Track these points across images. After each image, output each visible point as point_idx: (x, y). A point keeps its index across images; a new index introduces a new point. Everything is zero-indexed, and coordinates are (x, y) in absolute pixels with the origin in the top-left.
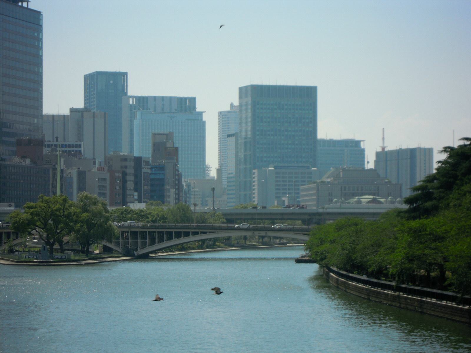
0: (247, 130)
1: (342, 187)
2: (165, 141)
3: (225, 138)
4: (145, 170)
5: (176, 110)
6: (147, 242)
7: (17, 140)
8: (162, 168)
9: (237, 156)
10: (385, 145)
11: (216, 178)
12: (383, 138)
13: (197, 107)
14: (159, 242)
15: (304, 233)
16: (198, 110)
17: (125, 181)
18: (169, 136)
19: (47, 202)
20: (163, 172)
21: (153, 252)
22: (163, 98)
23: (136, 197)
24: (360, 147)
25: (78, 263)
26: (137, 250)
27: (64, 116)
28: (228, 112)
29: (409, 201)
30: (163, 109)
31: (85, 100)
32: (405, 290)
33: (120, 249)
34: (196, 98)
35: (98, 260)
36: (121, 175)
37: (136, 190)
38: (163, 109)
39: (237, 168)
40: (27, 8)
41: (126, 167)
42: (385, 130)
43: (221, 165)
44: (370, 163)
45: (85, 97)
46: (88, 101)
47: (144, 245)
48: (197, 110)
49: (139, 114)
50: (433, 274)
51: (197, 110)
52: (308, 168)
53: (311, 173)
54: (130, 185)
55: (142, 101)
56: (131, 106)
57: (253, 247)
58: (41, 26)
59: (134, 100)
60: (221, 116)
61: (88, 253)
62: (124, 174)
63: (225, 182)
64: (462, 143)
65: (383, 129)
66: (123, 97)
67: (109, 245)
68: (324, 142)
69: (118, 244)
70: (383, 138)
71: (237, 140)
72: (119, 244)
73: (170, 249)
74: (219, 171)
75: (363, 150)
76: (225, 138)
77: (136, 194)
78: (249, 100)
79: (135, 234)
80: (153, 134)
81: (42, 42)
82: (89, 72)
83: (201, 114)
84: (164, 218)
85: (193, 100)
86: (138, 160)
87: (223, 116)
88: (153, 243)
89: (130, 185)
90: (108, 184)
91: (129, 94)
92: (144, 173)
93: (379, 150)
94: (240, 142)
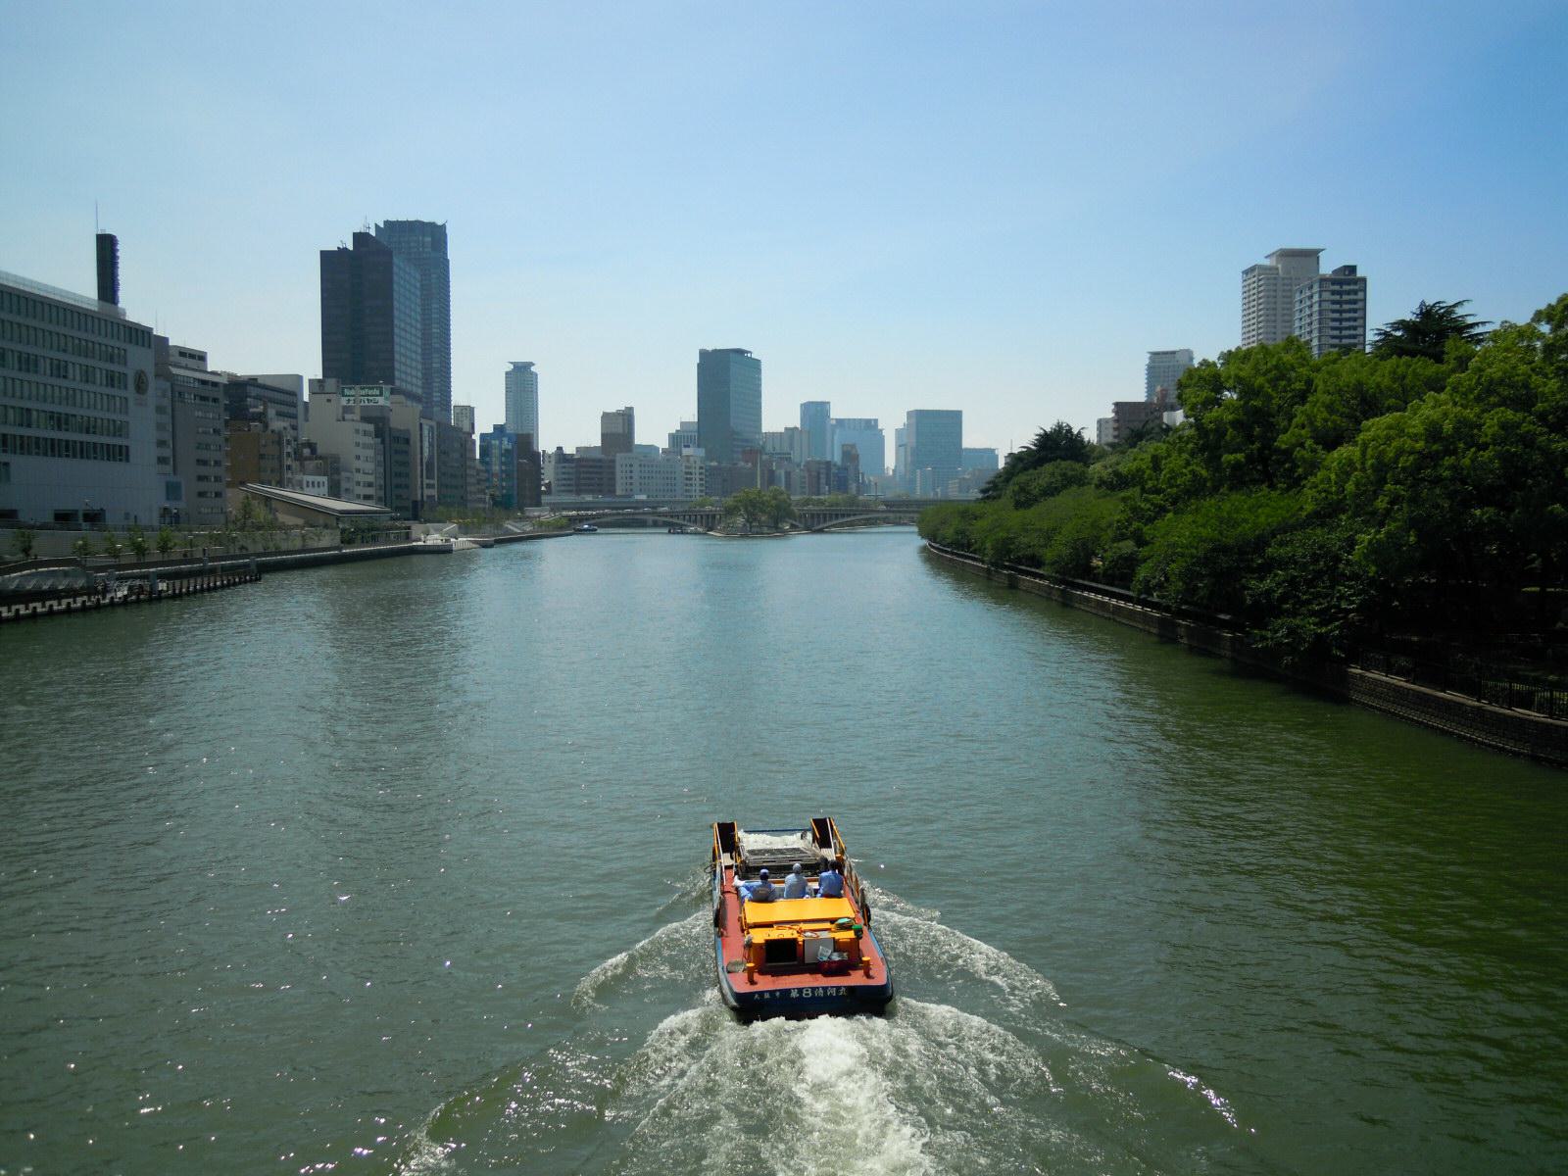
4: (834, 470)
7: (85, 521)
8: (846, 469)
16: (880, 427)
17: (819, 478)
18: (853, 446)
19: (747, 493)
21: (827, 528)
22: (849, 419)
25: (770, 536)
27: (781, 433)
29: (983, 491)
32: (956, 554)
33: (802, 526)
35: (784, 534)
37: (827, 484)
43: (896, 467)
47: (819, 523)
49: (838, 431)
52: (955, 468)
53: (957, 472)
54: (823, 481)
55: (840, 422)
56: (832, 425)
57: (905, 524)
61: (777, 528)
62: (819, 473)
63: (898, 479)
64: (1020, 450)
67: (794, 523)
68: (966, 449)
69: (800, 522)
73: (834, 526)
74: (894, 471)
78: (914, 420)
79: (812, 516)
83: (881, 430)
84: (837, 505)
85: (876, 421)
86: (828, 463)
88: (825, 521)
89: (823, 481)
91: (831, 417)
94: (909, 450)
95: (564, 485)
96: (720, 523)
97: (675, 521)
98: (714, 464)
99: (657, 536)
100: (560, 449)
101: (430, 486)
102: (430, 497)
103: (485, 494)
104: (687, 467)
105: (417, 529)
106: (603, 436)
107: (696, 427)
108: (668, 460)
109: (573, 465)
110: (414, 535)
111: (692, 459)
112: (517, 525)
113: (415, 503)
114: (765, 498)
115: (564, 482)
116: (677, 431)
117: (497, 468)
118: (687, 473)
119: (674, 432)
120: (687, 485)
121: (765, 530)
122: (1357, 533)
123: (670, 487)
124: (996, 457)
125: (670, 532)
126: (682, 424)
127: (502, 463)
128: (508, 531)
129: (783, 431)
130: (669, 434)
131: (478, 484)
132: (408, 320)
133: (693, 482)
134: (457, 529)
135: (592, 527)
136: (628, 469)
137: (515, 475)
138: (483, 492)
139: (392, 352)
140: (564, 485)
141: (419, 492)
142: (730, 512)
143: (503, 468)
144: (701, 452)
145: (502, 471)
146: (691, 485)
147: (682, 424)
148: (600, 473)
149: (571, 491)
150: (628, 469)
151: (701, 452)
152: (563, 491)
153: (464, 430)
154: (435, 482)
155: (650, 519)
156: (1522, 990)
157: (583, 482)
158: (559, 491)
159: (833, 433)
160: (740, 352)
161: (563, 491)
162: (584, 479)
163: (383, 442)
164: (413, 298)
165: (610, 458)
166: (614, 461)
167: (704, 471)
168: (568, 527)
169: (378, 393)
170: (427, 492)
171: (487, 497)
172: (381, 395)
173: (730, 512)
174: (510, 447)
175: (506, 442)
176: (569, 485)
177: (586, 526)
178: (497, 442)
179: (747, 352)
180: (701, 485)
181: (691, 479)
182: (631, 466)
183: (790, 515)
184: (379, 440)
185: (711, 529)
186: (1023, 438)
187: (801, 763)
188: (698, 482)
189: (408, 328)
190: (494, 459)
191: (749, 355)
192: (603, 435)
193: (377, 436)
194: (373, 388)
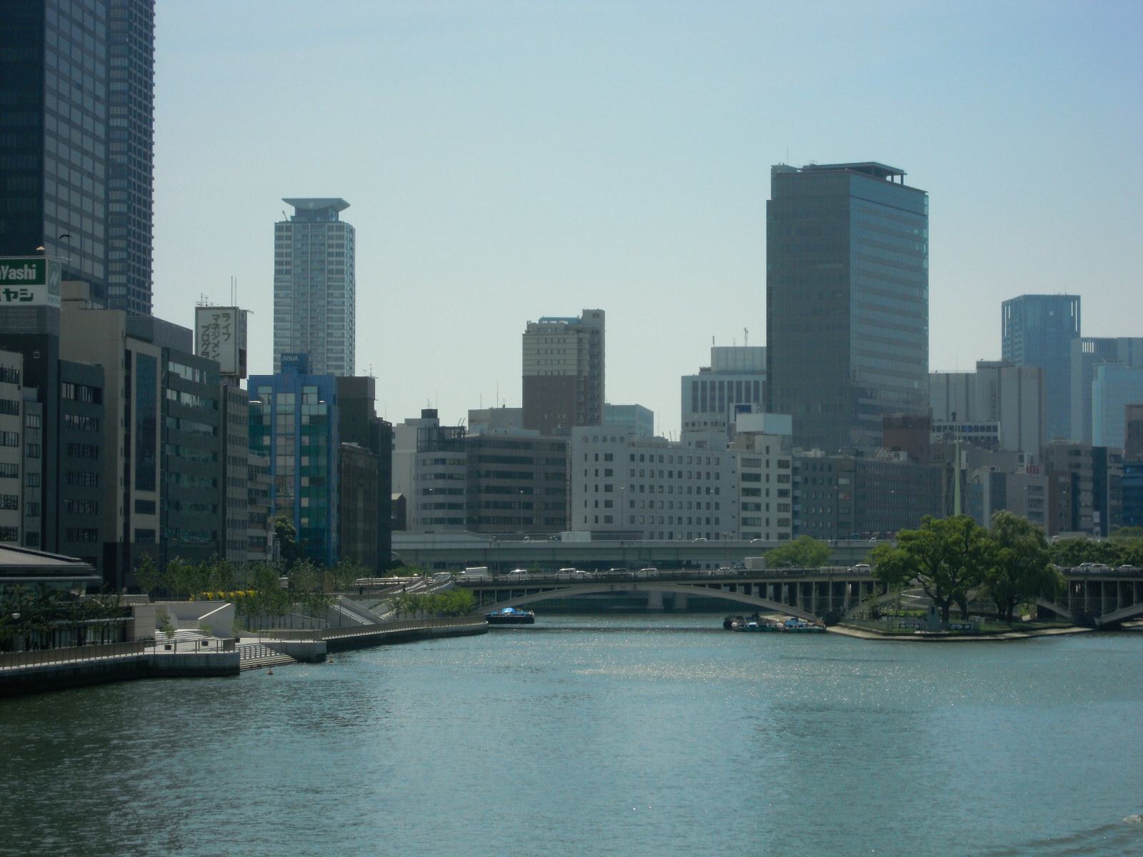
4: (1113, 471)
17: (1076, 492)
19: (938, 529)
23: (1097, 520)
26: (1099, 615)
27: (967, 375)
31: (1004, 347)
33: (1068, 614)
41: (1078, 466)
47: (1112, 607)
49: (1101, 370)
54: (1086, 498)
55: (1107, 347)
56: (1087, 356)
58: (926, 216)
61: (1011, 621)
62: (1076, 478)
67: (1047, 605)
69: (1064, 604)
77: (1097, 514)
79: (1094, 587)
86: (1100, 455)
89: (1086, 498)
90: (1046, 496)
91: (1084, 334)
95: (439, 506)
96: (854, 603)
97: (739, 597)
98: (816, 453)
99: (688, 636)
101: (145, 507)
102: (145, 535)
103: (265, 526)
104: (747, 462)
105: (144, 610)
106: (530, 384)
107: (761, 363)
108: (700, 444)
109: (463, 455)
110: (139, 632)
111: (759, 442)
112: (358, 604)
113: (110, 548)
114: (983, 542)
115: (440, 499)
116: (703, 370)
117: (291, 461)
118: (745, 477)
119: (696, 372)
120: (745, 507)
121: (983, 625)
122: (397, 614)
123: (704, 513)
125: (728, 626)
126: (717, 352)
127: (303, 451)
128: (341, 623)
129: (972, 369)
130: (684, 379)
131: (252, 502)
132: (76, 96)
133: (761, 485)
134: (232, 615)
135: (521, 613)
136: (602, 465)
137: (334, 481)
138: (262, 522)
139: (38, 173)
140: (439, 506)
141: (120, 521)
142: (892, 575)
143: (305, 461)
144: (783, 424)
145: (302, 471)
146: (758, 507)
147: (717, 352)
148: (528, 476)
149: (454, 521)
150: (602, 465)
151: (783, 424)
152: (439, 521)
153: (223, 368)
154: (155, 496)
155: (656, 592)
157: (485, 497)
158: (424, 521)
159: (1089, 376)
160: (875, 172)
161: (439, 521)
162: (489, 490)
163: (42, 398)
164: (89, 41)
165: (556, 438)
166: (562, 447)
167: (788, 472)
168: (469, 612)
169: (32, 274)
170: (140, 521)
171: (271, 534)
172: (40, 280)
173: (892, 575)
174: (323, 411)
175: (313, 398)
177: (508, 611)
178: (291, 398)
179: (893, 172)
180: (783, 508)
181: (756, 492)
182: (609, 457)
183: (1040, 584)
184: (32, 392)
185: (833, 623)
186: (699, 371)
188: (774, 500)
189: (77, 117)
190: (281, 441)
191: (897, 179)
192: (527, 380)
193: (28, 383)
194: (17, 265)
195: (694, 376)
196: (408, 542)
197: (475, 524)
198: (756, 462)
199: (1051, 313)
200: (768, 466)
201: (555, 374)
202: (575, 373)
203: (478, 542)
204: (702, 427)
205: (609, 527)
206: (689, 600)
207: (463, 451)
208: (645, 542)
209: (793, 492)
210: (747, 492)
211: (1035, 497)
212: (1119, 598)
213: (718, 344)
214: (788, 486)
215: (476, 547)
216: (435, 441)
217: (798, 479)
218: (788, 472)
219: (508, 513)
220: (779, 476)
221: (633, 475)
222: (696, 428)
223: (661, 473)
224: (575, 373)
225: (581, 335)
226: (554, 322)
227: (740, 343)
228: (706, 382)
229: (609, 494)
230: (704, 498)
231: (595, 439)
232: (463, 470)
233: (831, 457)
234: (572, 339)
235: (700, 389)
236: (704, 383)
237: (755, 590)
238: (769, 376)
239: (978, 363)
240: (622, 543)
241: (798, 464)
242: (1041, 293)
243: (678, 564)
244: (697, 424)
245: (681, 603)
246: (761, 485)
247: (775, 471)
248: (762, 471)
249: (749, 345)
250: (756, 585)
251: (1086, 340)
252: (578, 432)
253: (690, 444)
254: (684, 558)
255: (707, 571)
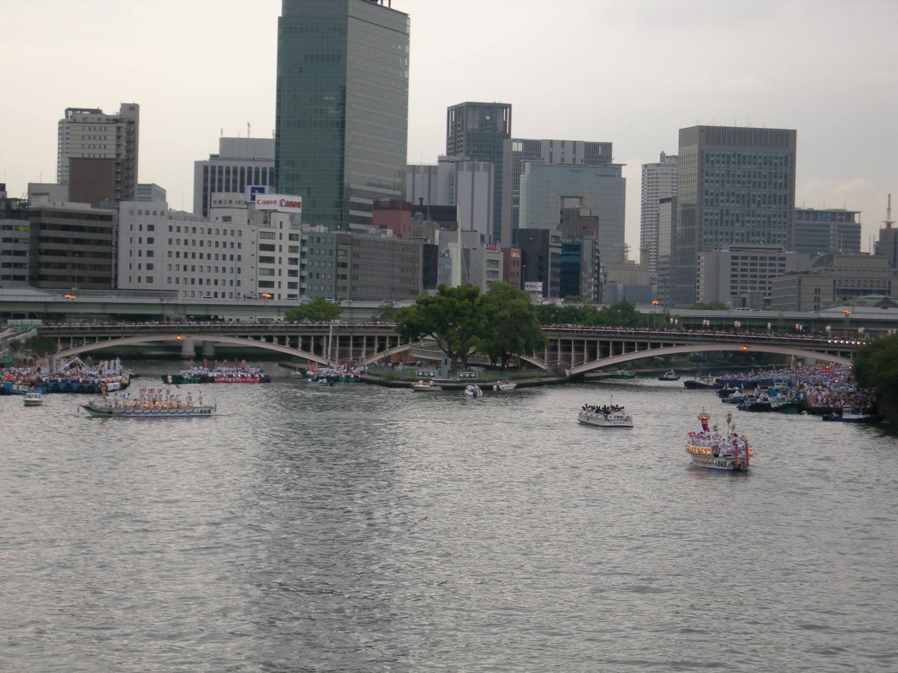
0: (689, 192)
1: (835, 281)
2: (577, 206)
3: (657, 204)
5: (582, 161)
6: (570, 356)
9: (674, 231)
10: (891, 220)
11: (638, 262)
12: (889, 209)
13: (613, 157)
14: (390, 348)
15: (816, 349)
20: (577, 253)
23: (540, 289)
24: (854, 221)
26: (569, 368)
28: (658, 165)
30: (563, 159)
31: (448, 144)
34: (124, 102)
36: (519, 256)
38: (563, 159)
39: (673, 250)
40: (389, 9)
42: (892, 197)
44: (867, 245)
45: (448, 139)
46: (453, 146)
48: (614, 162)
49: (528, 165)
50: (868, 407)
51: (614, 162)
55: (533, 147)
56: (517, 153)
58: (408, 35)
59: (521, 145)
60: (646, 171)
65: (889, 195)
66: (505, 141)
70: (889, 209)
71: (674, 207)
72: (542, 357)
75: (859, 227)
76: (657, 204)
78: (694, 149)
80: (71, 159)
81: (408, 58)
82: (456, 103)
83: (619, 167)
85: (608, 147)
87: (649, 170)
90: (500, 269)
91: (514, 136)
92: (552, 253)
93: (884, 226)
94: (679, 209)
100: (663, 155)
116: (213, 157)
119: (207, 158)
123: (228, 276)
124: (856, 230)
130: (197, 164)
133: (275, 254)
136: (145, 234)
149: (17, 278)
150: (145, 234)
156: (203, 552)
167: (297, 243)
176: (16, 265)
181: (271, 260)
182: (151, 228)
187: (25, 546)
195: (205, 161)
196: (25, 296)
197: (36, 280)
198: (271, 235)
199: (488, 118)
200: (281, 238)
201: (97, 156)
202: (114, 156)
203: (41, 296)
204: (228, 205)
205: (150, 286)
206: (216, 348)
207: (27, 219)
208: (180, 300)
209: (301, 261)
210: (263, 259)
211: (493, 269)
212: (585, 354)
213: (226, 135)
214: (297, 255)
215: (18, 300)
216: (3, 210)
217: (305, 249)
218: (297, 243)
219: (62, 272)
220: (290, 247)
221: (239, 244)
222: (223, 205)
223: (178, 241)
224: (114, 156)
225: (119, 125)
226: (86, 113)
227: (244, 135)
228: (222, 167)
229: (150, 258)
230: (228, 264)
231: (140, 212)
232: (27, 235)
233: (331, 232)
234: (113, 128)
235: (224, 173)
236: (213, 167)
237: (276, 339)
238: (277, 163)
239: (439, 157)
240: (162, 300)
241: (306, 237)
242: (476, 101)
243: (207, 318)
244: (223, 202)
245: (209, 352)
246: (275, 254)
247: (286, 243)
248: (276, 242)
249: (251, 137)
250: (264, 337)
251: (516, 140)
252: (124, 205)
253: (217, 219)
254: (213, 314)
255: (595, 305)
